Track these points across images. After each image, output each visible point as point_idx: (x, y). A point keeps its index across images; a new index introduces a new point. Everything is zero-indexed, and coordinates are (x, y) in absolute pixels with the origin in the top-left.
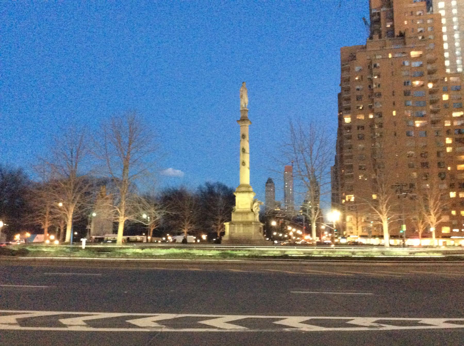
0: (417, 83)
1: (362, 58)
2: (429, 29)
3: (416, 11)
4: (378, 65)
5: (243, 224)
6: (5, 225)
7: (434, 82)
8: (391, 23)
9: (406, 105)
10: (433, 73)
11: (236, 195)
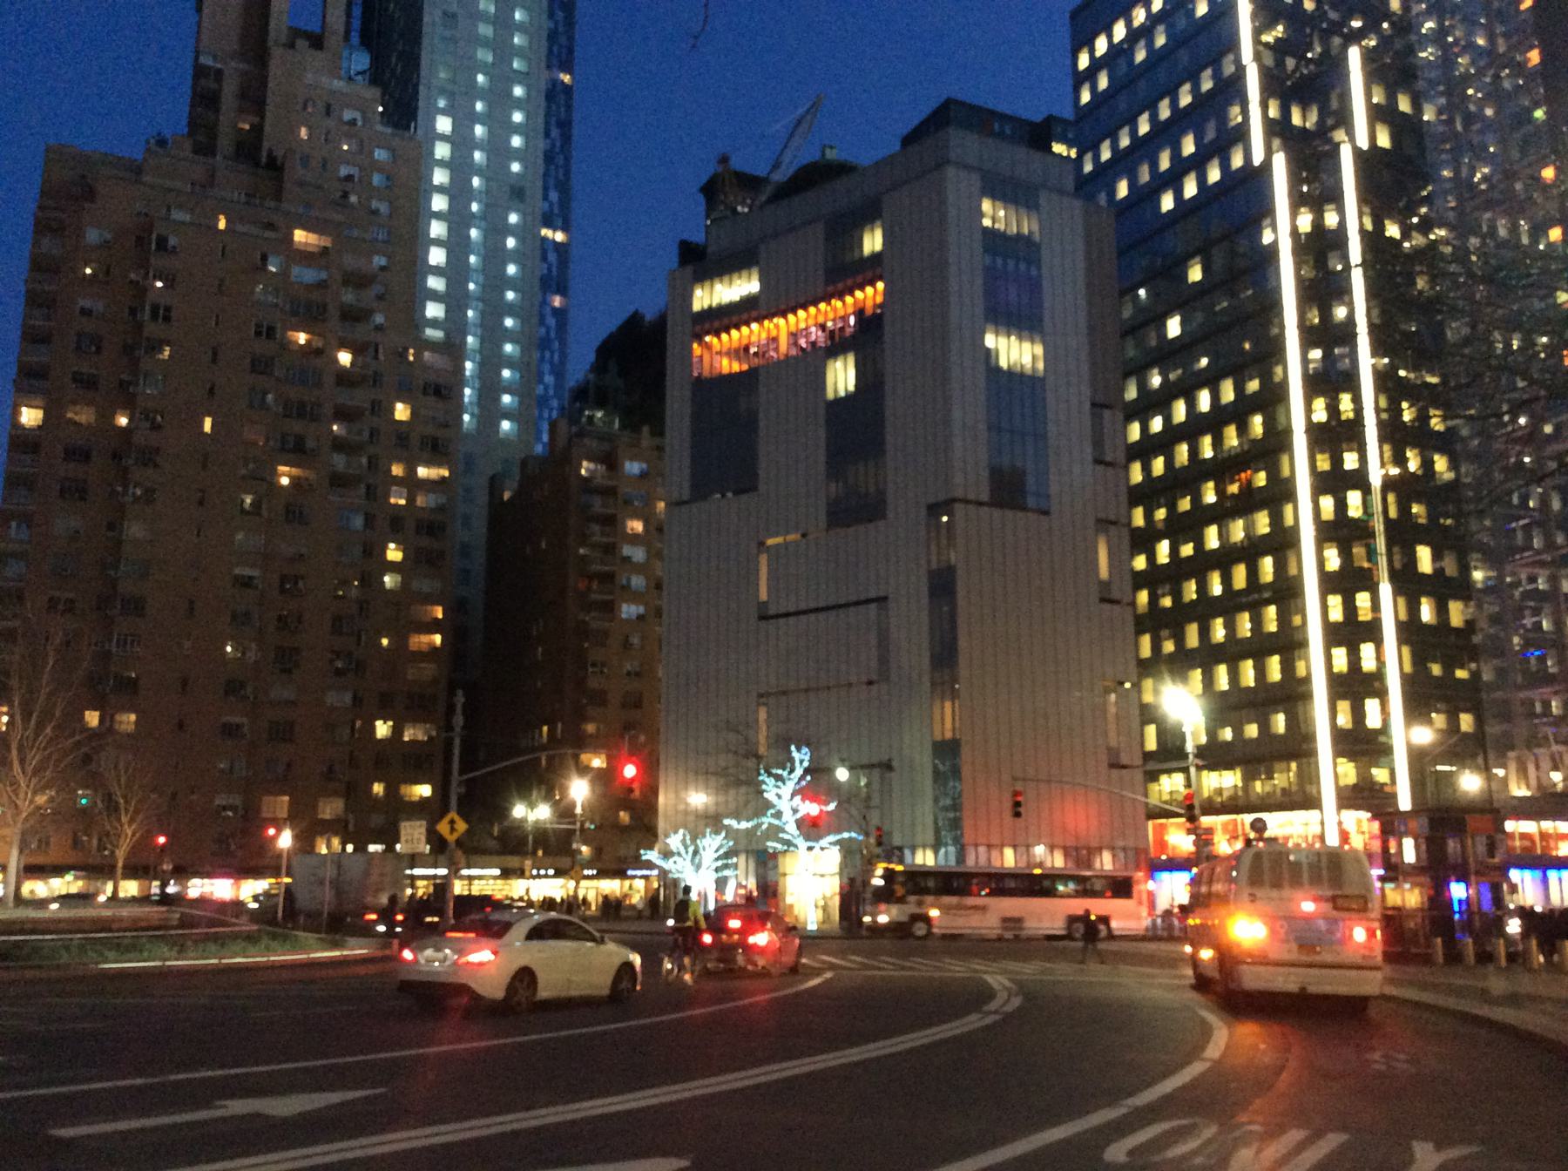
2: (377, 179)
4: (172, 241)
6: (769, 925)
8: (256, 120)
10: (357, 319)
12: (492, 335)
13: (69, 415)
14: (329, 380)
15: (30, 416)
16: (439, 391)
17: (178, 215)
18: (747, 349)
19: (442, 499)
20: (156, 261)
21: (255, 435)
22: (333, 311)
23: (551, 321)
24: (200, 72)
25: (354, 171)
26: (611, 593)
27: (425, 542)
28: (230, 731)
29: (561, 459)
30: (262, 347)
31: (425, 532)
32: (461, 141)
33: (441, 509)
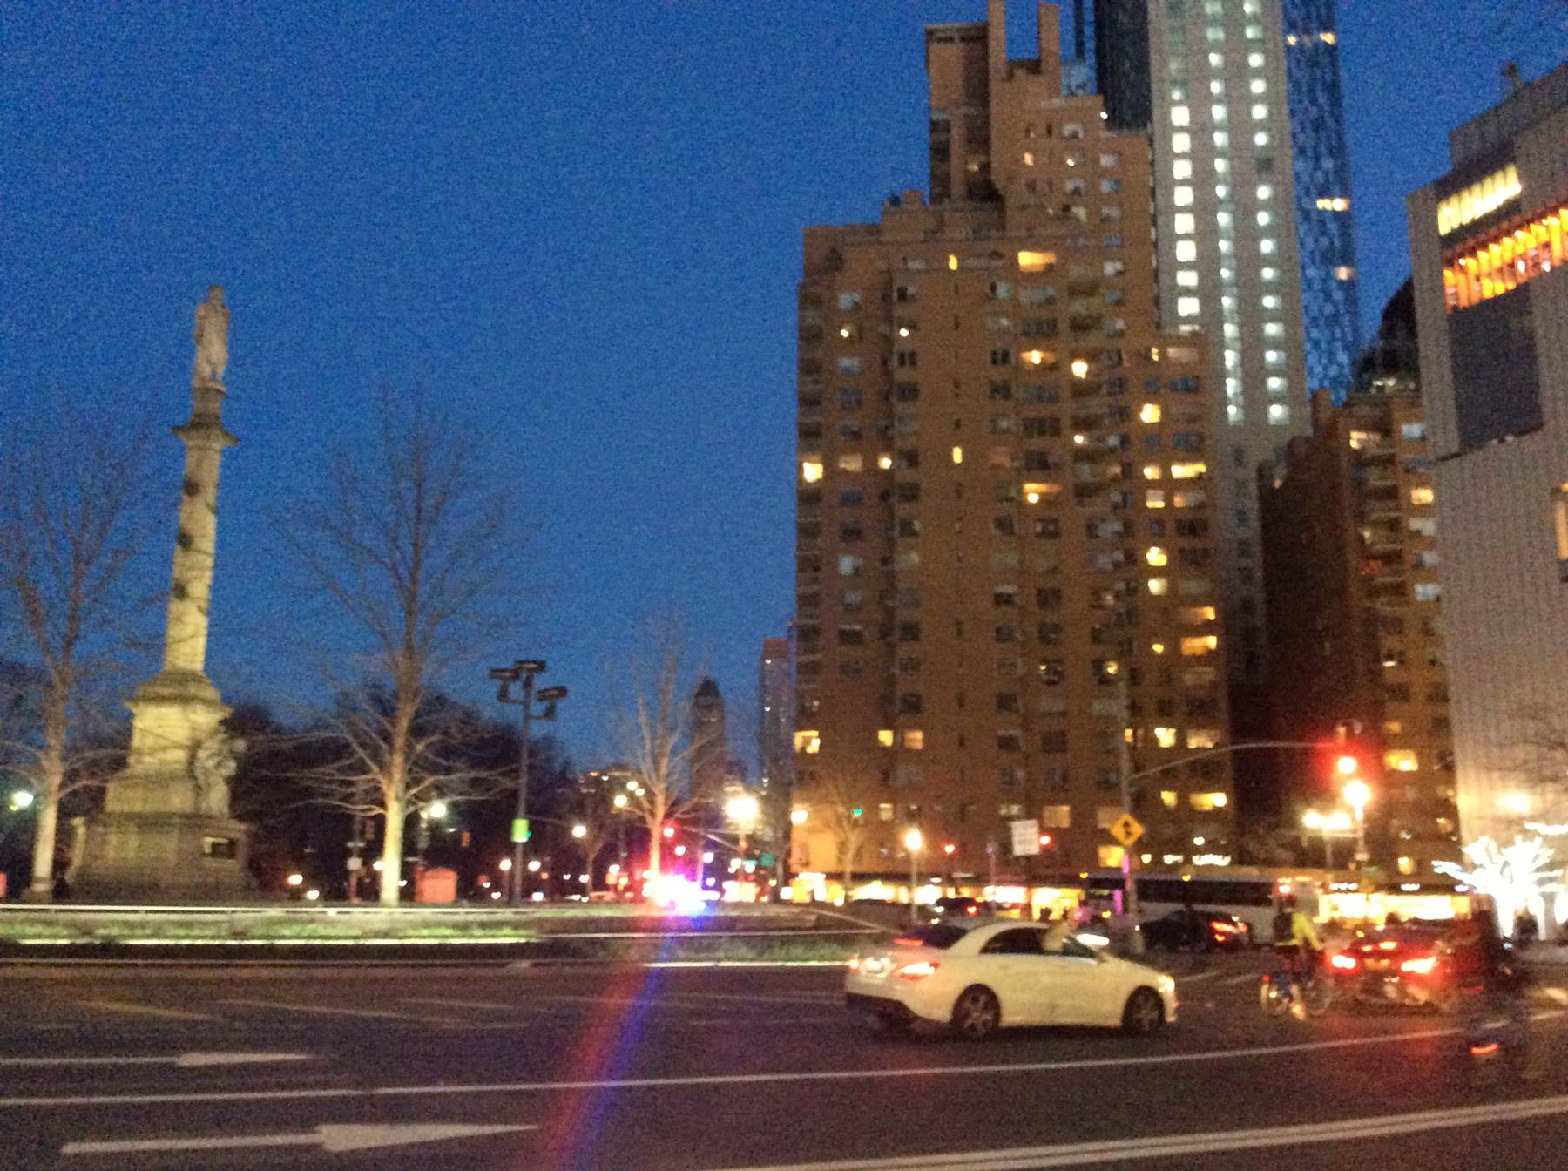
0: (1035, 357)
1: (864, 264)
2: (1105, 187)
3: (1061, 126)
4: (911, 290)
5: (139, 826)
7: (1091, 357)
8: (983, 158)
9: (994, 431)
11: (134, 710)
12: (1251, 317)
13: (842, 465)
14: (1065, 393)
15: (813, 472)
16: (1193, 386)
17: (915, 265)
18: (1512, 265)
19: (1201, 496)
20: (900, 311)
21: (1001, 457)
22: (1063, 326)
23: (1338, 296)
24: (935, 126)
25: (1080, 183)
26: (1397, 573)
27: (1187, 543)
28: (1007, 744)
29: (1327, 433)
30: (998, 374)
31: (1187, 532)
32: (1200, 129)
33: (1200, 507)
